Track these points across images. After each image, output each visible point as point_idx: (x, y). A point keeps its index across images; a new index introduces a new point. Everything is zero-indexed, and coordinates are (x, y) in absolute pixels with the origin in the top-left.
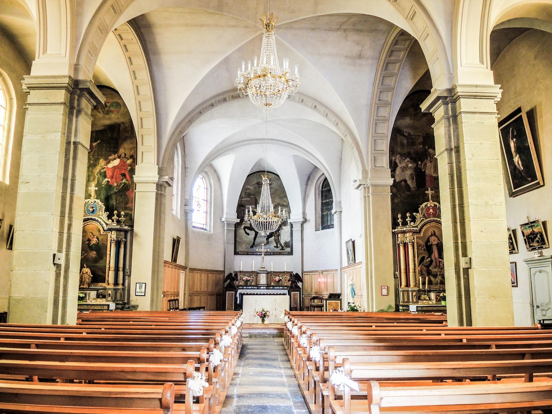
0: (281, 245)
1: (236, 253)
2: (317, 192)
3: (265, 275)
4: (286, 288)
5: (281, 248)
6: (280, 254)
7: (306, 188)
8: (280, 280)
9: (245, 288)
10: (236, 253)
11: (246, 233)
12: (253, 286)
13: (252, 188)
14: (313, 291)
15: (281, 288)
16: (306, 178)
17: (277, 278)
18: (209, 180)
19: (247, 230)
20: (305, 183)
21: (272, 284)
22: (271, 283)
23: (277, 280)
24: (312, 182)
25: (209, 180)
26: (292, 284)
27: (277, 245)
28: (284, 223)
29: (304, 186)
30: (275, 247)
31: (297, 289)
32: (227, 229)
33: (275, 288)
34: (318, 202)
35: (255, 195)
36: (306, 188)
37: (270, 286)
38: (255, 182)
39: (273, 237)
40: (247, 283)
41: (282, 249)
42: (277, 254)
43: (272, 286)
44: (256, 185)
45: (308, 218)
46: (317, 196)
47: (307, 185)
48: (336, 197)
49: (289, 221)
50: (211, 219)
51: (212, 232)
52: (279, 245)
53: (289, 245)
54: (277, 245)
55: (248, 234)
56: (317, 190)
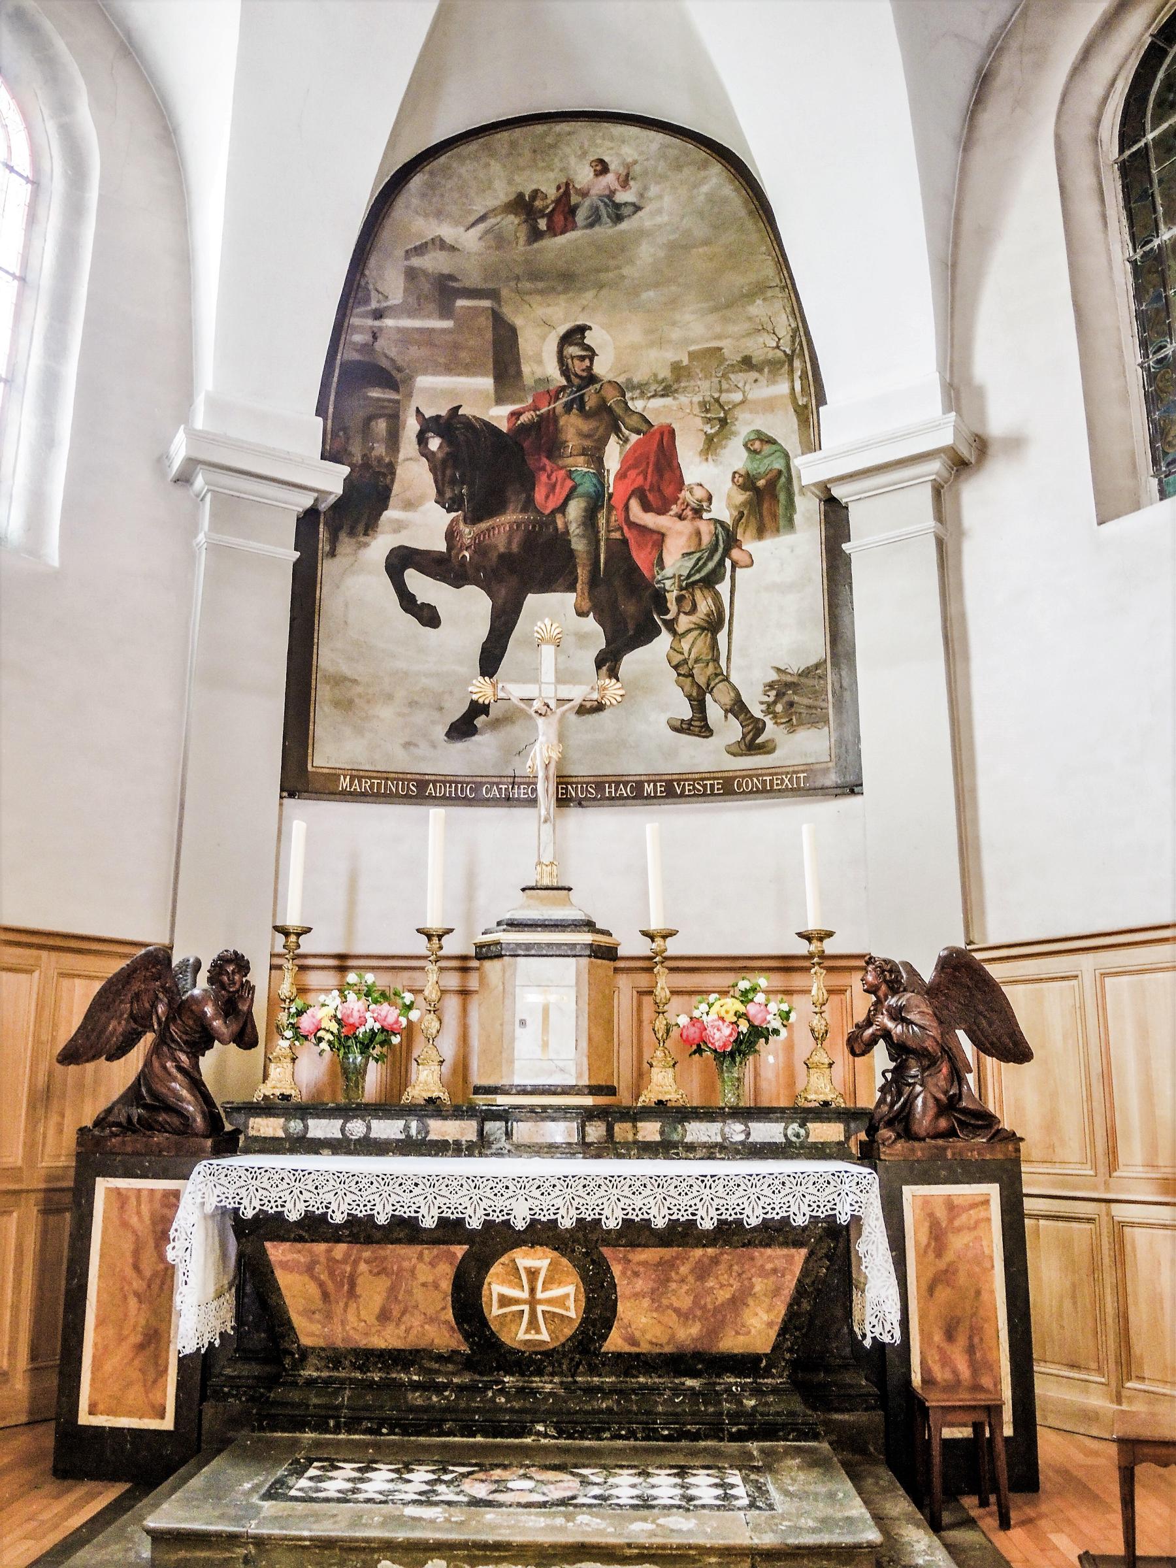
0: (738, 708)
1: (299, 779)
2: (1084, 180)
3: (569, 970)
4: (829, 1132)
5: (733, 730)
6: (726, 788)
7: (963, 172)
8: (759, 1033)
9: (321, 1128)
10: (299, 779)
11: (408, 601)
12: (432, 1108)
13: (470, 240)
14: (1132, 1153)
15: (767, 1132)
16: (960, 86)
17: (718, 1017)
18: (63, 108)
19: (414, 580)
20: (953, 120)
21: (663, 1085)
22: (641, 1077)
23: (721, 1036)
24: (1022, 102)
25: (63, 108)
26: (897, 1081)
27: (699, 706)
28: (766, 499)
29: (948, 151)
30: (682, 728)
31: (975, 1146)
32: (215, 549)
33: (699, 1132)
34: (1094, 262)
35: (493, 294)
36: (963, 172)
37: (634, 1115)
38: (502, 193)
39: (664, 640)
40: (351, 1076)
41: (752, 744)
42: (706, 795)
43: (661, 1110)
44: (512, 222)
45: (999, 421)
46: (1087, 210)
47: (967, 140)
48: (551, 1074)
49: (809, 470)
50: (46, 441)
51: (53, 553)
52: (714, 712)
53: (814, 691)
54: (699, 706)
55: (429, 617)
56: (1081, 158)
